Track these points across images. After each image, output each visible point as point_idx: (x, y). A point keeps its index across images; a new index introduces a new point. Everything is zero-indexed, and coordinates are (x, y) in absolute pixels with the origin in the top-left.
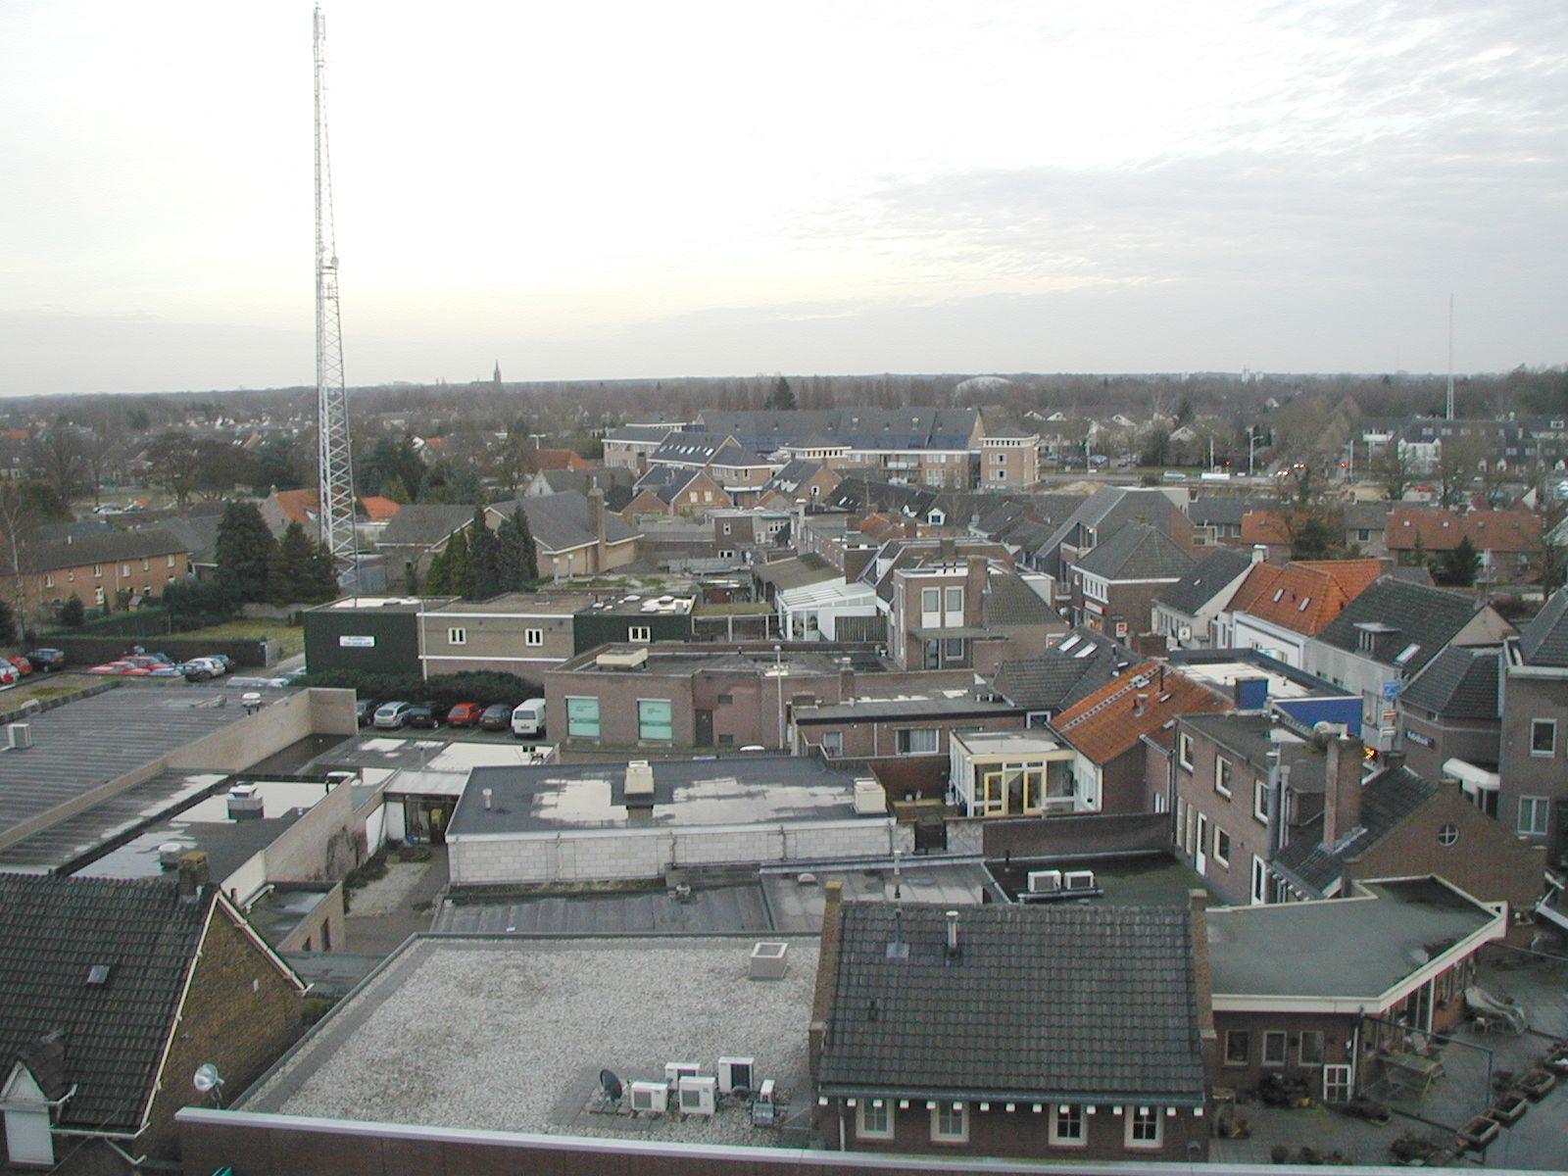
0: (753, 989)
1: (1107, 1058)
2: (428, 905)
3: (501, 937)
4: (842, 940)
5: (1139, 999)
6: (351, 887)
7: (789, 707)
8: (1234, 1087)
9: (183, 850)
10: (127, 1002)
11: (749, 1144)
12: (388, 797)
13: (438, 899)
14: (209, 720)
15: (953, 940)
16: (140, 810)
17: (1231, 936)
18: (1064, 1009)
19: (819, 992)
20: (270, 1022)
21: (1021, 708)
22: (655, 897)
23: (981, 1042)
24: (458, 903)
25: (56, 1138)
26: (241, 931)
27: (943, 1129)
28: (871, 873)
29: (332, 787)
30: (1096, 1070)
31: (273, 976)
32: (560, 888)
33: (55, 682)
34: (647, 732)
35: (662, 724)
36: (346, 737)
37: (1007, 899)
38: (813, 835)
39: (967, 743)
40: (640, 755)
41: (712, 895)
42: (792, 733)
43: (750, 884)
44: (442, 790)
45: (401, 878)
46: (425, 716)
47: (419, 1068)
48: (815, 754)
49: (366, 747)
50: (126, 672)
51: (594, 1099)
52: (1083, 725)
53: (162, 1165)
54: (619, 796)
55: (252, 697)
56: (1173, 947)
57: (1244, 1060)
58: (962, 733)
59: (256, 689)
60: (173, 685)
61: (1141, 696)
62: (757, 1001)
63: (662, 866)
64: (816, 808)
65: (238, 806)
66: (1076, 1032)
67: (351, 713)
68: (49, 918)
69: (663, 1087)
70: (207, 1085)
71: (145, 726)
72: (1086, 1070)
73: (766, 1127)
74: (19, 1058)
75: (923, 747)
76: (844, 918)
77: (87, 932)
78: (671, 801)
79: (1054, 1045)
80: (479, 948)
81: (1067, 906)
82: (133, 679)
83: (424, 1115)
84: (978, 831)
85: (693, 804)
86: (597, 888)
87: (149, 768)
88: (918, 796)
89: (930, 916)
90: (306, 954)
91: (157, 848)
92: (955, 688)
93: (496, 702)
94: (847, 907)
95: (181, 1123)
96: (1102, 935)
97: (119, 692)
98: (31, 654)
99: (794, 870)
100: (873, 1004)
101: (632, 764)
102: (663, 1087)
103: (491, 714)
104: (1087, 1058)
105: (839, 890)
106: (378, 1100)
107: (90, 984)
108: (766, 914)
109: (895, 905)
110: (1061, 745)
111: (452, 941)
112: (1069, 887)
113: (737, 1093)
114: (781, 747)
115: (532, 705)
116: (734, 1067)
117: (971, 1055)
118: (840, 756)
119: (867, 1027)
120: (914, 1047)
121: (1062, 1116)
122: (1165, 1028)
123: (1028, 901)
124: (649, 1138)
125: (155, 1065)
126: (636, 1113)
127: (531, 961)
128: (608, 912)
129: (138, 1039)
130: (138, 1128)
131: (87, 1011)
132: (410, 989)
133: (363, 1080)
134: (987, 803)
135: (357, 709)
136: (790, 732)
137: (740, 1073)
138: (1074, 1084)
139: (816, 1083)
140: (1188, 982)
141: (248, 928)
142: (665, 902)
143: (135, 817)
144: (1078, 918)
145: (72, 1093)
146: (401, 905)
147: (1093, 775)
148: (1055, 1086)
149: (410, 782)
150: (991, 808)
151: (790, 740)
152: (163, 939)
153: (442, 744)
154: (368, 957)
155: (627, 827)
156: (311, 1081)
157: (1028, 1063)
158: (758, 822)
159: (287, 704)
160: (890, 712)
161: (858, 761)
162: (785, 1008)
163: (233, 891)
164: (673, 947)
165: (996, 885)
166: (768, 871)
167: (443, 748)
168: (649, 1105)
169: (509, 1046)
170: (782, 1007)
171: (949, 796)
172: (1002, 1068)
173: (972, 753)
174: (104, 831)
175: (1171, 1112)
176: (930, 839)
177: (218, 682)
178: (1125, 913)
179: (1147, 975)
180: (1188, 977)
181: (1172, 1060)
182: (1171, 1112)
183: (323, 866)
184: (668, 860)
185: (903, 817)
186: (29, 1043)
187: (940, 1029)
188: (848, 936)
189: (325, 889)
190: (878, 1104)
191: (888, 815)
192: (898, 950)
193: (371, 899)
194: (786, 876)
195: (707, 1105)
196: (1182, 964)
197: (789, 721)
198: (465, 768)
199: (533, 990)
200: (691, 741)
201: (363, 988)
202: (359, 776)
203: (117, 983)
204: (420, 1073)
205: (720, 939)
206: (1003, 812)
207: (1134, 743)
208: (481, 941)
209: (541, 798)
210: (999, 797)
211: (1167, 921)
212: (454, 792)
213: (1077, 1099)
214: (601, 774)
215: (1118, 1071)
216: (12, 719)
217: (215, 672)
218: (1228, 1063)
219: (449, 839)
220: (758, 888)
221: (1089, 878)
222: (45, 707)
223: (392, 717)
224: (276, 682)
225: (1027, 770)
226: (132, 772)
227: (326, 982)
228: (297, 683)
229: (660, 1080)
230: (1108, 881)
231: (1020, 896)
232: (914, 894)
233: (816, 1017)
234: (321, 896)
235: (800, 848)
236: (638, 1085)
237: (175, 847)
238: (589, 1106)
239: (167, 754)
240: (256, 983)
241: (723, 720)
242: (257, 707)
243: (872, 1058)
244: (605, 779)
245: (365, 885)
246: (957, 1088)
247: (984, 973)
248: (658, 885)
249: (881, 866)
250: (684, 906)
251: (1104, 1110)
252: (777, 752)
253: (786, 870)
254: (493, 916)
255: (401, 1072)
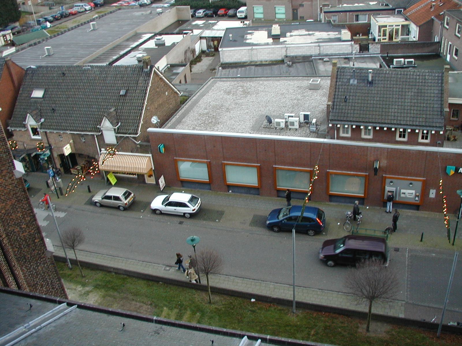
0: (310, 92)
1: (415, 115)
2: (214, 69)
3: (236, 78)
4: (337, 78)
5: (426, 98)
6: (192, 64)
7: (321, 8)
8: (453, 126)
9: (143, 56)
10: (131, 100)
11: (309, 137)
12: (201, 38)
13: (217, 67)
14: (147, 18)
15: (370, 79)
16: (130, 45)
17: (456, 80)
18: (403, 100)
19: (330, 94)
20: (171, 104)
21: (394, 8)
22: (281, 65)
23: (377, 109)
24: (223, 68)
25: (116, 137)
26: (161, 78)
27: (365, 134)
28: (345, 58)
29: (185, 35)
30: (411, 119)
31: (171, 91)
32: (253, 63)
33: (101, 9)
34: (278, 16)
35: (282, 14)
36: (187, 21)
37: (387, 67)
38: (328, 47)
39: (376, 19)
40: (276, 23)
41: (298, 65)
42: (322, 16)
43: (309, 61)
44: (217, 35)
45: (206, 61)
46: (211, 14)
47: (213, 116)
48: (329, 22)
49: (194, 23)
50: (122, 5)
51: (264, 124)
52: (413, 13)
53: (145, 144)
54: (270, 36)
55: (159, 10)
56: (438, 83)
57: (457, 118)
58: (375, 15)
59: (160, 8)
60: (136, 8)
61: (434, 4)
62: (311, 96)
63: (283, 56)
64: (330, 39)
65: (158, 43)
66: (406, 108)
67: (189, 13)
68: (108, 77)
69: (284, 120)
70: (155, 122)
71: (129, 21)
72: (408, 119)
73: (314, 132)
74: (104, 116)
75: (363, 20)
76: (338, 72)
77: (119, 80)
78: (285, 37)
79: (399, 111)
80: (230, 81)
81: (405, 69)
82: (124, 7)
83: (216, 129)
84: (379, 46)
85: (292, 38)
86: (264, 63)
87: (131, 33)
88: (361, 35)
89: (364, 71)
90: (180, 84)
91: (136, 56)
92: (373, 1)
93: (232, 8)
94: (338, 68)
95: (149, 132)
96: (416, 79)
97: (121, 11)
98: (94, 2)
99: (322, 57)
100: (346, 97)
101: (274, 26)
102: (284, 120)
103: (231, 12)
104: (409, 115)
105: (336, 63)
106: (203, 125)
107: (121, 95)
108: (314, 71)
109: (353, 68)
110: (406, 20)
111: (222, 79)
112: (406, 64)
113: (305, 122)
114: (319, 20)
115: (243, 9)
116: (304, 115)
117: (374, 113)
118: (337, 23)
119: (344, 104)
120: (358, 110)
121: (400, 132)
122: (433, 107)
123: (393, 68)
124: (280, 135)
125: (140, 116)
126: (276, 128)
127: (245, 85)
128: (268, 69)
129: (135, 110)
130: (137, 134)
131: (121, 103)
132: (210, 93)
133: (198, 120)
134: (382, 38)
135: (191, 12)
136: (321, 16)
137: (306, 117)
138: (405, 123)
139: (328, 120)
140: (442, 94)
141: (163, 77)
142: (284, 67)
143: (129, 47)
144: (409, 73)
145: (119, 125)
146: (207, 69)
147: (416, 29)
148: (399, 123)
149: (208, 33)
150: (383, 39)
151: (321, 18)
152: (140, 82)
153: (216, 21)
154: (198, 85)
155: (272, 45)
156: (184, 120)
157: (391, 116)
158: (311, 43)
159: (170, 12)
160: (353, 9)
161: (342, 24)
162: (319, 98)
163: (158, 67)
164: (286, 80)
165: (384, 63)
166: (315, 58)
167: (217, 23)
168: (280, 126)
169: (239, 109)
170: (318, 98)
171: (370, 35)
172: (383, 117)
173: (378, 22)
174: (120, 52)
175: (433, 132)
176: (364, 48)
177: (149, 6)
178: (424, 72)
179: (429, 91)
180: (442, 92)
181: (435, 117)
182: (433, 132)
183: (183, 59)
184: (285, 54)
185: (356, 41)
186: (107, 112)
187: (365, 105)
188: (339, 77)
189: (185, 66)
190: (346, 126)
191: (351, 41)
192: (354, 81)
193: (198, 68)
194: (320, 59)
195: (297, 126)
196: (440, 88)
197: (321, 12)
198: (224, 29)
199: (246, 93)
200: (291, 19)
201: (197, 93)
202: (192, 32)
203: (128, 95)
204: (214, 117)
205: (300, 78)
206: (387, 40)
207: (430, 19)
208: (230, 79)
209: (247, 37)
210: (386, 36)
211: (436, 75)
212: (220, 36)
213: (405, 127)
214: (264, 29)
215: (418, 120)
216: (91, 21)
217: (148, 3)
218: (452, 119)
219: (220, 49)
220: (312, 63)
221: (412, 61)
222: (100, 17)
223: (201, 14)
224: (166, 5)
225: (395, 27)
226: (127, 34)
227: (187, 92)
228: (172, 5)
229: (283, 119)
230: (419, 62)
231: (391, 66)
232: (358, 65)
233: (329, 101)
234: (184, 67)
235: (324, 51)
236: (277, 120)
237: (141, 55)
238: (263, 126)
239: (136, 29)
240: (167, 93)
241: (301, 12)
242: (161, 13)
243: (345, 113)
244: (266, 30)
245: (196, 64)
246: (370, 122)
247: (379, 89)
248: (282, 62)
249: (349, 56)
250: (290, 68)
251: (413, 131)
252: (317, 21)
253: (320, 57)
254: (234, 71)
255: (209, 117)
